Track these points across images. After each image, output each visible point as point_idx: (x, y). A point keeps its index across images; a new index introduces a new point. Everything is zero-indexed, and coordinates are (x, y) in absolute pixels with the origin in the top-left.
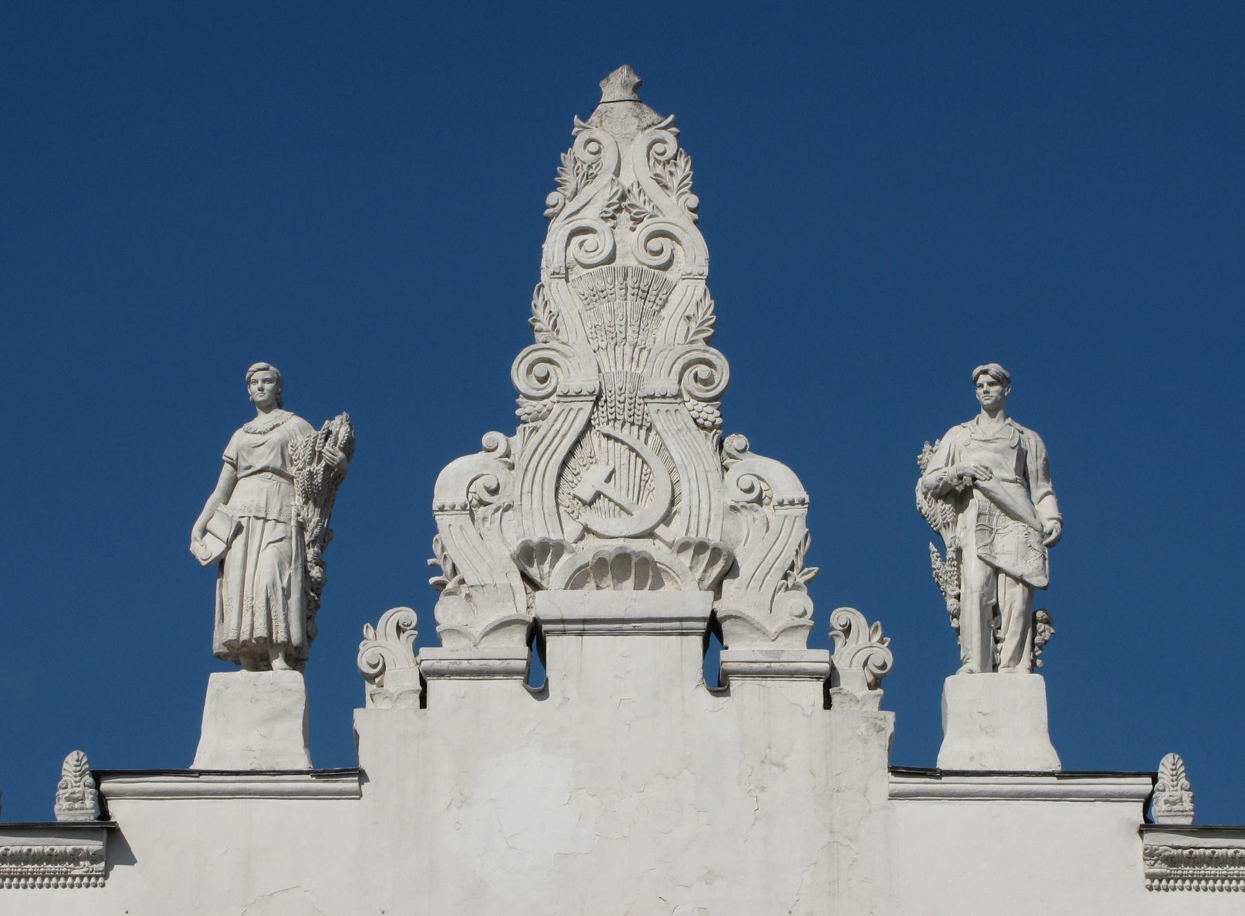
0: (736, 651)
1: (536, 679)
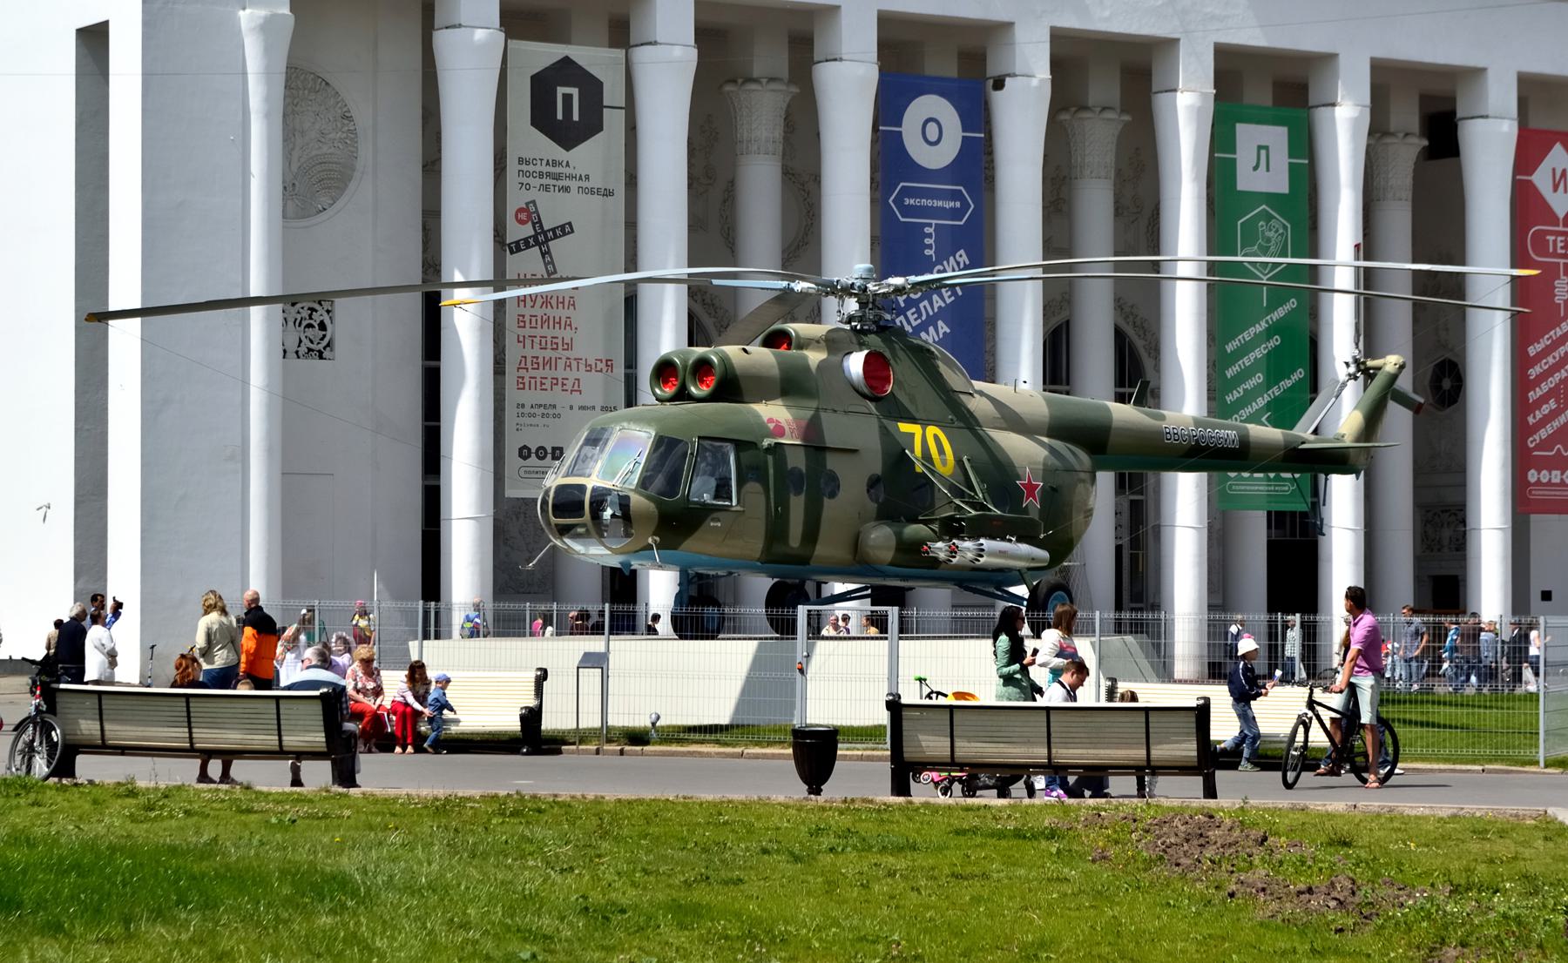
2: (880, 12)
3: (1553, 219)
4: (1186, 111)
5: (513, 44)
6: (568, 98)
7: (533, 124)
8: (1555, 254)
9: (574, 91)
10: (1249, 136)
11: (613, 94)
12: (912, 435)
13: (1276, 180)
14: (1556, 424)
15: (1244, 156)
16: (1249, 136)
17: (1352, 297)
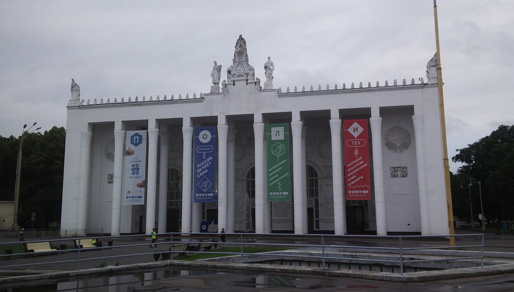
1: (234, 85)
3: (354, 138)
6: (136, 139)
7: (503, 129)
8: (354, 145)
9: (138, 137)
11: (144, 137)
14: (356, 181)
15: (273, 134)
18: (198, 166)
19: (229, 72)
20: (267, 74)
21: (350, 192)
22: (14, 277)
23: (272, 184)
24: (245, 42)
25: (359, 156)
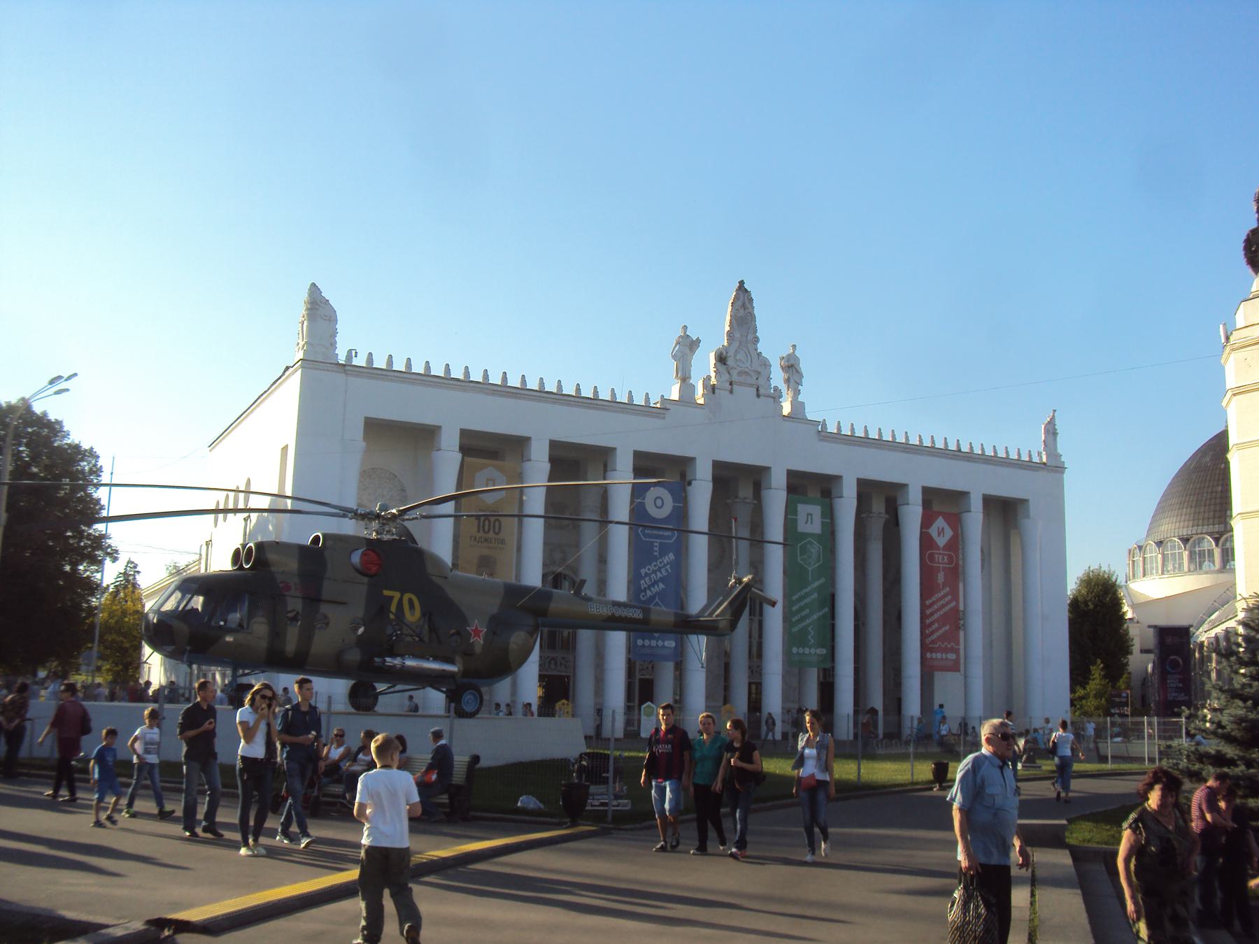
0: (762, 391)
1: (731, 392)
2: (614, 449)
3: (938, 548)
4: (776, 500)
5: (468, 459)
10: (803, 509)
12: (392, 598)
13: (815, 527)
16: (803, 509)
17: (452, 519)
18: (643, 571)
19: (721, 359)
20: (792, 381)
21: (929, 655)
22: (507, 891)
23: (795, 629)
24: (751, 300)
25: (944, 585)
